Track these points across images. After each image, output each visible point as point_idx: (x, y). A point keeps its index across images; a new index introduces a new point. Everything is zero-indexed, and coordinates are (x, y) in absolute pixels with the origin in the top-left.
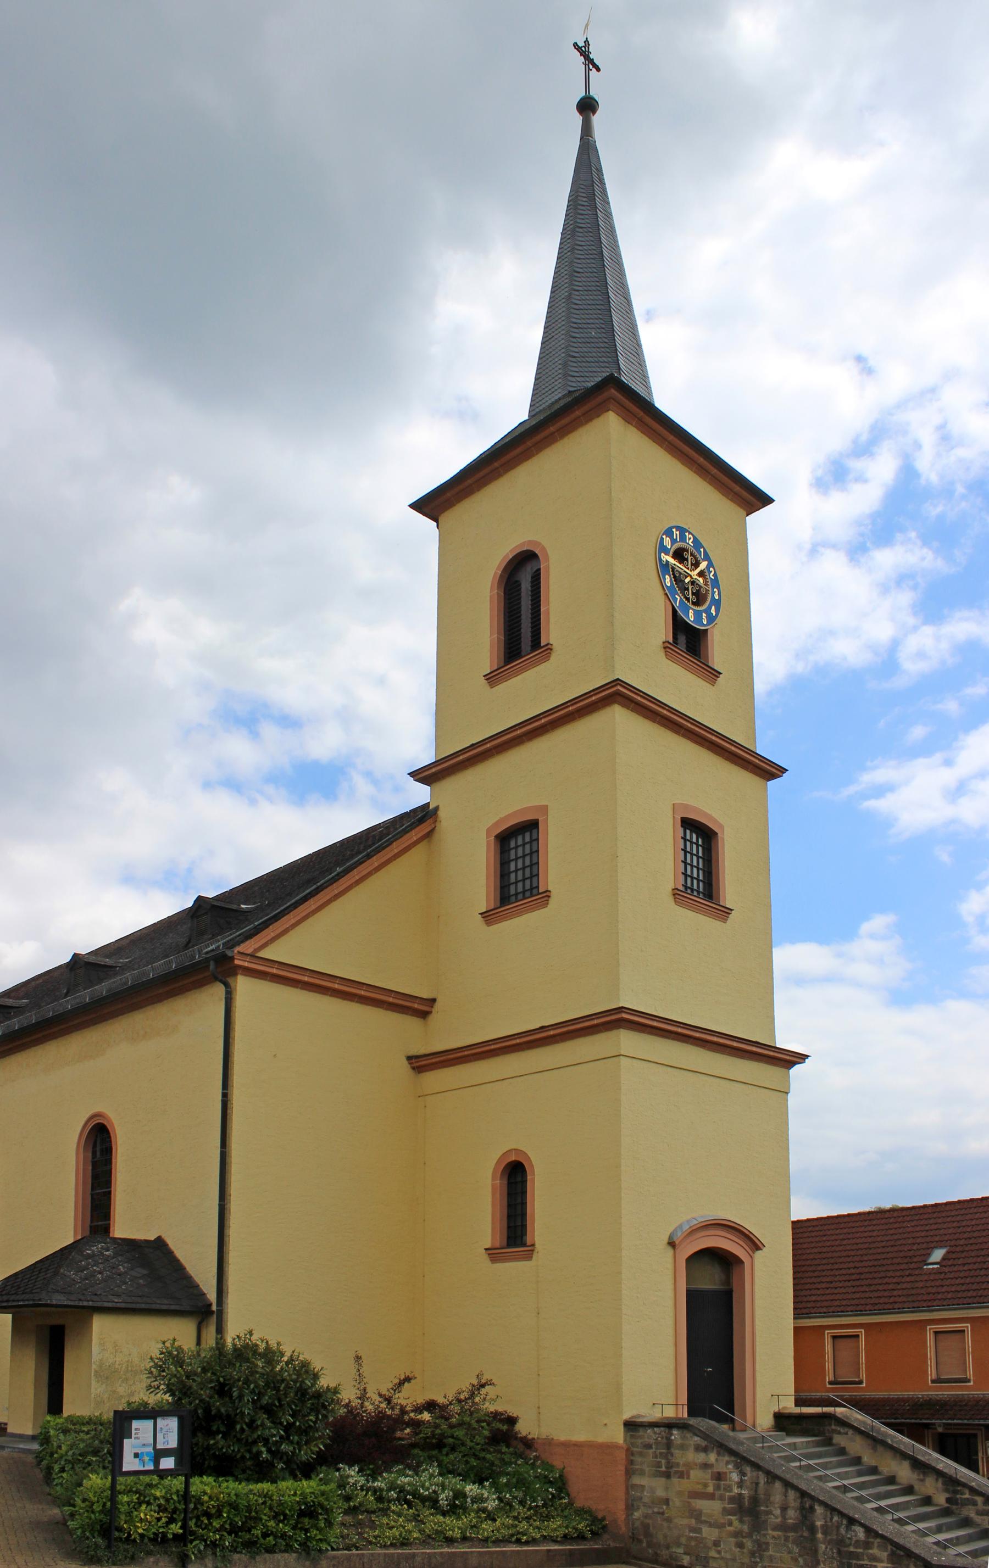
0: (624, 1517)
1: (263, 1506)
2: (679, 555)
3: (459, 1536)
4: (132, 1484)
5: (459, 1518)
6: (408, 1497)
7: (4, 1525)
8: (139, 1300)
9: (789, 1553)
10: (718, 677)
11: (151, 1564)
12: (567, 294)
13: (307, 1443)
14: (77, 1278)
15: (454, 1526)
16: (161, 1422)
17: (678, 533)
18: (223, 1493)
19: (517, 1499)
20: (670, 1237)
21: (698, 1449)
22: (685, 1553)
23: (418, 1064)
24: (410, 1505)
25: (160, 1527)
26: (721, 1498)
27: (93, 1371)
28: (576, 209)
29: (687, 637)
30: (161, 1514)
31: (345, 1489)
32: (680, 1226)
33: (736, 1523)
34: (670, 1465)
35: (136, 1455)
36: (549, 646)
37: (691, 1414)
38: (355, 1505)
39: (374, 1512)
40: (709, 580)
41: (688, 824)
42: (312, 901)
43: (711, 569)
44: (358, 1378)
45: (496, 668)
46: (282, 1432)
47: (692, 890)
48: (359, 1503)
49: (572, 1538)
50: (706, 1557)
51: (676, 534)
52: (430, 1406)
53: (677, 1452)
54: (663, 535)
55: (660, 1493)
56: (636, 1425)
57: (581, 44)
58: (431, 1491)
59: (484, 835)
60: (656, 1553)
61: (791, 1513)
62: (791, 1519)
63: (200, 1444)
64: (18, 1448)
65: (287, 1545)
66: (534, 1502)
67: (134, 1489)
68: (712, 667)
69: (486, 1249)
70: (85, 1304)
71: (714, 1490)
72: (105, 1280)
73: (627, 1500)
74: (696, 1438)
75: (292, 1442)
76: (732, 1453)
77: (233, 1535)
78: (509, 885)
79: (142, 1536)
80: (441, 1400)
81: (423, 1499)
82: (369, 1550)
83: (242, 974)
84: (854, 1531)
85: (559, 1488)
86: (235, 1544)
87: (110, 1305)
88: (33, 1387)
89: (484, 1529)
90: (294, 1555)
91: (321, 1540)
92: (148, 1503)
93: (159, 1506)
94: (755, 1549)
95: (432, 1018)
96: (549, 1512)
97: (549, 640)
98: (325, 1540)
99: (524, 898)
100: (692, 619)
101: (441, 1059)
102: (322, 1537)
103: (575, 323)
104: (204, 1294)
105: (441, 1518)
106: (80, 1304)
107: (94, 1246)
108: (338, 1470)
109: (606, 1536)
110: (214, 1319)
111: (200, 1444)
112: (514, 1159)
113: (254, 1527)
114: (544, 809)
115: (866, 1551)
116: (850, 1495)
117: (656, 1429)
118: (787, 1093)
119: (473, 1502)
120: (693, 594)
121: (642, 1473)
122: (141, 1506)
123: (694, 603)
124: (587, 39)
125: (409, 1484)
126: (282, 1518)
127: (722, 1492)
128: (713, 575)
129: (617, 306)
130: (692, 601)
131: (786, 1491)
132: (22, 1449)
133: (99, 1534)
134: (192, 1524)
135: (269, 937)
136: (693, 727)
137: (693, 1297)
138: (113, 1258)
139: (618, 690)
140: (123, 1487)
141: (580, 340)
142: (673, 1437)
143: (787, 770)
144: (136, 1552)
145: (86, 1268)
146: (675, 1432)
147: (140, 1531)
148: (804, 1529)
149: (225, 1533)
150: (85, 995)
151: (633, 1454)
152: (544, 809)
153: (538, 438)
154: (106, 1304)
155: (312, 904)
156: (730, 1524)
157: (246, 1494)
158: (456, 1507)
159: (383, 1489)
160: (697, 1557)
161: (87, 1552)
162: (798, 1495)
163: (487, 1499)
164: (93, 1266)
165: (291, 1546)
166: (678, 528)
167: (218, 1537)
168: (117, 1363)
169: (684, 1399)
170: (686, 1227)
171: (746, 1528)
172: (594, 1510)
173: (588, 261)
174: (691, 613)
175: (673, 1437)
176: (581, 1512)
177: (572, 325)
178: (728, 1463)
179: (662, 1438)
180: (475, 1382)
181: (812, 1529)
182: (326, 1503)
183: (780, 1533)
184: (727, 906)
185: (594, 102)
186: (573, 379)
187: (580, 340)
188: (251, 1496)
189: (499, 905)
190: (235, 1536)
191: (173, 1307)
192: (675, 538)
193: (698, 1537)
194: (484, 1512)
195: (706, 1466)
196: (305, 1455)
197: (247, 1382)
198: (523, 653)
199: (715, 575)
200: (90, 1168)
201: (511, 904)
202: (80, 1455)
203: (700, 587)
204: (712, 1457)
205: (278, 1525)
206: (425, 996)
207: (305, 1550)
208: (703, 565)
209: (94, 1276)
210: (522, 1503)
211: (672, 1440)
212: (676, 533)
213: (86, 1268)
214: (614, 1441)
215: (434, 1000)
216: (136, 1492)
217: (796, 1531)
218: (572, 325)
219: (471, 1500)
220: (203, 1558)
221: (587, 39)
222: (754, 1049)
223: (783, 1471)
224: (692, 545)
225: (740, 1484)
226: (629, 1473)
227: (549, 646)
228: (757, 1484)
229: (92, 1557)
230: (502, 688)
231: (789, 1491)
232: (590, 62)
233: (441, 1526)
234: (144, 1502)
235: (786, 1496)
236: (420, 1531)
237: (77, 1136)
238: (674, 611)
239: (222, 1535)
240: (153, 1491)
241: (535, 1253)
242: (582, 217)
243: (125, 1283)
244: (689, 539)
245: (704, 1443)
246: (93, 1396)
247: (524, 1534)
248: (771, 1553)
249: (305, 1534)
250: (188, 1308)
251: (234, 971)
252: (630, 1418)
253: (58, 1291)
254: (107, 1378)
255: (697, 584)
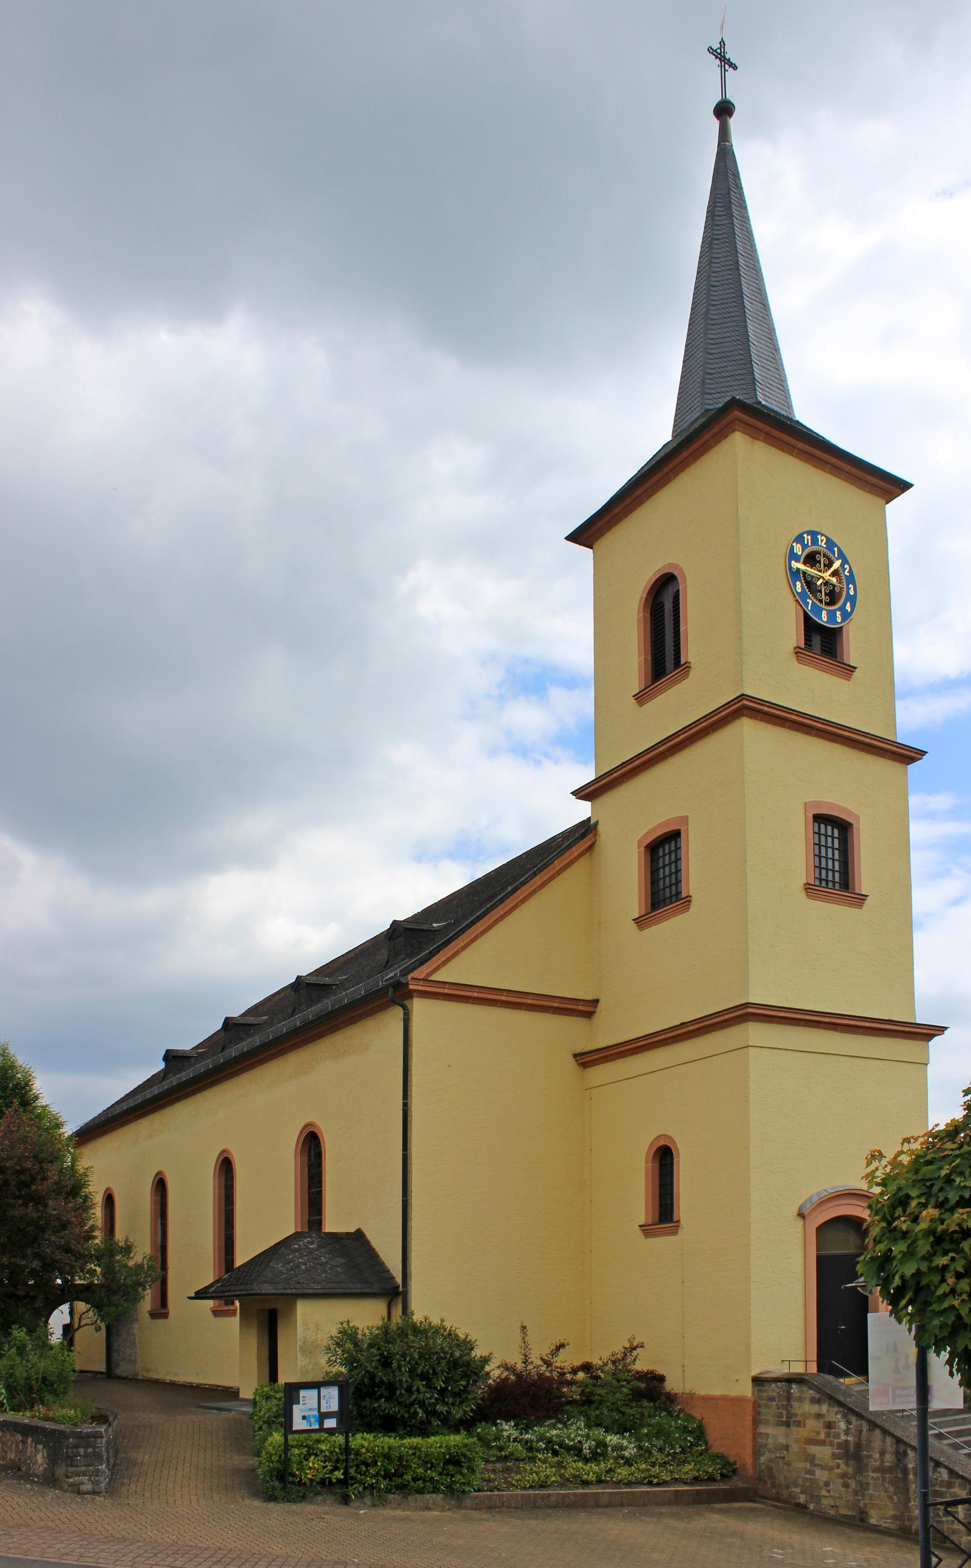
0: (751, 1461)
1: (413, 1457)
2: (811, 559)
3: (594, 1479)
4: (303, 1440)
5: (598, 1464)
6: (554, 1447)
7: (211, 1471)
8: (336, 1285)
9: (886, 1492)
10: (853, 672)
11: (319, 1501)
12: (704, 310)
13: (461, 1403)
14: (285, 1271)
15: (591, 1470)
16: (324, 1391)
17: (809, 537)
18: (378, 1447)
19: (656, 1447)
20: (800, 1209)
21: (814, 1401)
22: (801, 1493)
23: (582, 1061)
24: (555, 1453)
25: (325, 1473)
26: (831, 1444)
27: (298, 1347)
28: (713, 220)
29: (821, 637)
30: (327, 1463)
31: (499, 1441)
32: (810, 1198)
33: (843, 1466)
34: (789, 1416)
35: (304, 1418)
36: (687, 665)
37: (821, 1368)
38: (506, 1455)
39: (523, 1460)
40: (843, 578)
41: (819, 819)
42: (479, 924)
43: (846, 566)
44: (523, 1345)
45: (643, 688)
46: (436, 1395)
47: (827, 881)
48: (510, 1453)
49: (703, 1480)
50: (818, 1496)
51: (808, 539)
52: (586, 1367)
53: (795, 1404)
54: (793, 542)
55: (782, 1440)
56: (763, 1381)
57: (716, 46)
58: (576, 1441)
59: (635, 846)
60: (778, 1492)
61: (888, 1457)
62: (888, 1462)
63: (368, 1407)
64: (242, 1411)
65: (434, 1487)
66: (672, 1449)
67: (304, 1444)
68: (848, 663)
69: (640, 1226)
70: (289, 1291)
71: (825, 1437)
72: (308, 1270)
73: (754, 1447)
74: (811, 1392)
75: (447, 1404)
76: (840, 1404)
77: (388, 1480)
78: (659, 891)
79: (311, 1480)
80: (596, 1361)
81: (569, 1449)
82: (510, 1491)
83: (417, 997)
84: (939, 1472)
85: (698, 1436)
86: (389, 1487)
87: (310, 1291)
88: (256, 1360)
89: (619, 1474)
90: (441, 1495)
91: (464, 1484)
92: (316, 1455)
93: (325, 1456)
94: (858, 1488)
95: (596, 1017)
96: (686, 1458)
97: (687, 658)
98: (468, 1483)
99: (671, 903)
100: (825, 620)
101: (602, 1055)
102: (464, 1481)
103: (712, 339)
104: (394, 1278)
105: (580, 1464)
106: (286, 1292)
107: (300, 1241)
108: (496, 1425)
109: (735, 1478)
110: (400, 1300)
111: (368, 1407)
112: (662, 1144)
113: (406, 1474)
114: (685, 820)
115: (949, 1490)
116: (945, 1442)
117: (778, 1384)
118: (926, 1064)
119: (613, 1450)
120: (826, 594)
121: (767, 1423)
122: (310, 1457)
123: (827, 604)
124: (722, 39)
125: (557, 1436)
126: (429, 1466)
127: (831, 1439)
128: (848, 572)
129: (753, 314)
130: (825, 602)
131: (885, 1437)
132: (245, 1411)
133: (277, 1478)
134: (352, 1471)
135: (440, 961)
136: (823, 726)
137: (823, 1263)
138: (317, 1250)
139: (744, 704)
140: (295, 1443)
141: (716, 356)
142: (792, 1391)
143: (927, 752)
144: (306, 1492)
145: (292, 1261)
146: (794, 1386)
147: (309, 1476)
148: (898, 1470)
149: (380, 1478)
150: (310, 1013)
151: (759, 1406)
152: (685, 820)
153: (672, 465)
154: (307, 1291)
155: (479, 926)
156: (838, 1467)
157: (399, 1447)
158: (598, 1453)
159: (533, 1440)
160: (812, 1495)
161: (267, 1492)
162: (894, 1441)
163: (627, 1447)
164: (298, 1259)
165: (438, 1489)
166: (809, 533)
167: (374, 1481)
168: (319, 1339)
169: (813, 1355)
170: (815, 1199)
171: (850, 1470)
172: (726, 1455)
173: (724, 273)
174: (824, 614)
175: (792, 1391)
176: (714, 1458)
177: (708, 341)
178: (837, 1413)
179: (783, 1392)
180: (628, 1345)
181: (905, 1471)
182: (468, 1453)
183: (878, 1475)
184: (863, 893)
185: (732, 106)
186: (710, 397)
187: (716, 356)
188: (403, 1449)
189: (650, 911)
190: (389, 1481)
191: (365, 1291)
192: (806, 543)
193: (812, 1478)
194: (622, 1459)
195: (819, 1416)
196: (457, 1413)
197: (404, 1356)
198: (667, 672)
199: (850, 571)
200: (307, 1170)
201: (667, 906)
202: (275, 1418)
203: (834, 586)
204: (824, 1408)
205: (426, 1471)
206: (590, 998)
207: (450, 1491)
208: (837, 564)
209: (299, 1267)
210: (661, 1450)
211: (791, 1393)
212: (807, 538)
213: (292, 1261)
214: (744, 1395)
215: (597, 1001)
216: (306, 1446)
217: (891, 1473)
218: (708, 341)
219: (612, 1449)
220: (362, 1498)
221: (722, 39)
222: (888, 1027)
223: (884, 1420)
224: (825, 546)
225: (847, 1432)
226: (756, 1422)
227: (687, 665)
228: (861, 1431)
229: (271, 1496)
230: (650, 706)
231: (887, 1438)
232: (725, 62)
233: (579, 1471)
234: (313, 1454)
235: (884, 1442)
236: (560, 1476)
237: (295, 1144)
238: (807, 617)
239: (378, 1480)
240: (319, 1446)
241: (680, 1228)
242: (719, 228)
243: (325, 1272)
244: (822, 541)
245: (817, 1396)
246: (299, 1367)
247: (655, 1477)
248: (871, 1492)
249: (451, 1479)
250: (378, 1291)
251: (410, 995)
252: (758, 1374)
253: (266, 1282)
254: (310, 1352)
255: (831, 584)
